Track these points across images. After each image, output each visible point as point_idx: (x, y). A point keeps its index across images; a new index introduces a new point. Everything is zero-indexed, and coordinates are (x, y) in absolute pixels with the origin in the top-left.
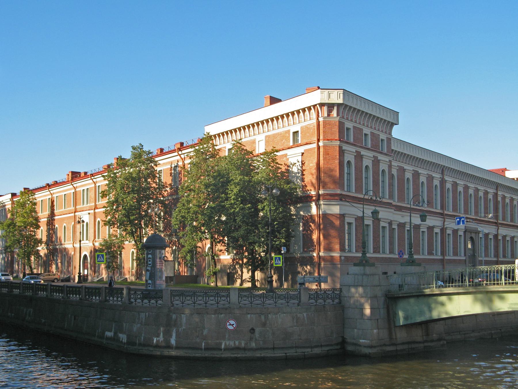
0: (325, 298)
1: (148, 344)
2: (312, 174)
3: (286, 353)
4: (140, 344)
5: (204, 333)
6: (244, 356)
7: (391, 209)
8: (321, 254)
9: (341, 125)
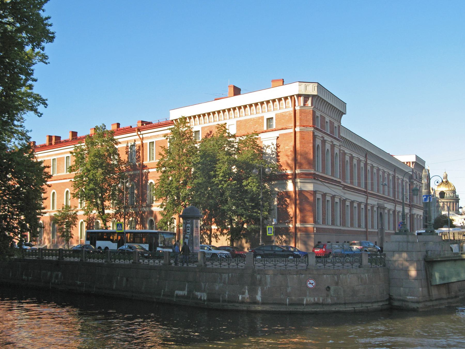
0: (343, 262)
1: (234, 301)
2: (287, 156)
3: (354, 308)
4: (224, 301)
5: (288, 291)
6: (322, 310)
7: (341, 186)
8: (298, 225)
9: (314, 112)
